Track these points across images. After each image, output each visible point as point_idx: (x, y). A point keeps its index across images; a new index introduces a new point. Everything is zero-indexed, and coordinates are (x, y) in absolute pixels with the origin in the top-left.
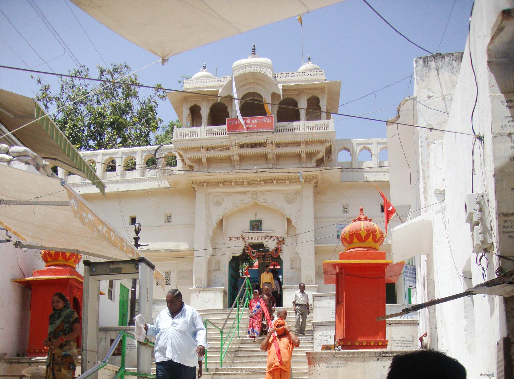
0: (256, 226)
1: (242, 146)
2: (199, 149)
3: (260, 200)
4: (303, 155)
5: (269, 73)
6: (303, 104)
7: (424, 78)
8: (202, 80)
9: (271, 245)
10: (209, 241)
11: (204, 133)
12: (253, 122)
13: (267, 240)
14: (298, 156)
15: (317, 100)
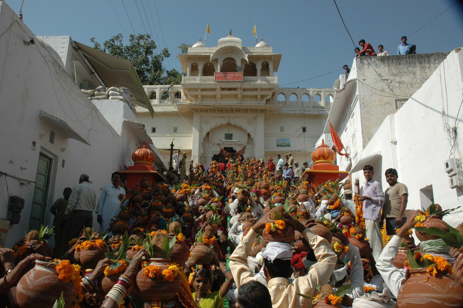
1: (223, 89)
2: (197, 90)
3: (233, 122)
4: (259, 97)
5: (240, 47)
6: (259, 67)
7: (361, 69)
8: (196, 48)
11: (198, 80)
14: (256, 97)
15: (267, 64)
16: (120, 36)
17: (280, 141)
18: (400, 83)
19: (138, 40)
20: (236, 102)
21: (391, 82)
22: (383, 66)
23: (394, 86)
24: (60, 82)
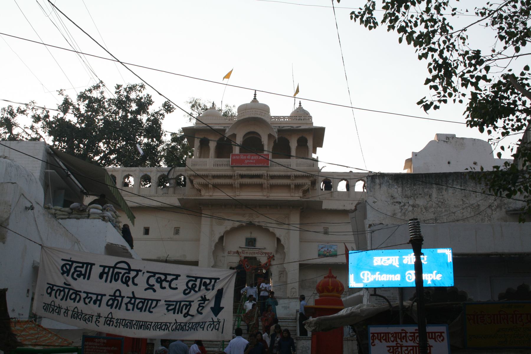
0: (251, 242)
2: (207, 176)
6: (293, 145)
9: (263, 260)
10: (212, 254)
12: (252, 158)
13: (260, 255)
15: (306, 141)
16: (101, 85)
17: (322, 248)
18: (413, 206)
19: (128, 92)
20: (260, 194)
21: (404, 205)
22: (396, 187)
23: (407, 210)
24: (300, 105)
